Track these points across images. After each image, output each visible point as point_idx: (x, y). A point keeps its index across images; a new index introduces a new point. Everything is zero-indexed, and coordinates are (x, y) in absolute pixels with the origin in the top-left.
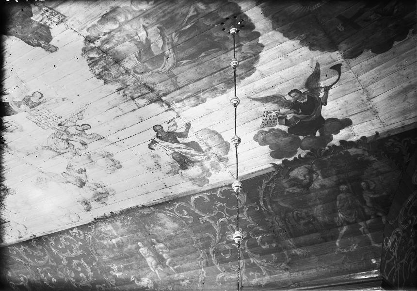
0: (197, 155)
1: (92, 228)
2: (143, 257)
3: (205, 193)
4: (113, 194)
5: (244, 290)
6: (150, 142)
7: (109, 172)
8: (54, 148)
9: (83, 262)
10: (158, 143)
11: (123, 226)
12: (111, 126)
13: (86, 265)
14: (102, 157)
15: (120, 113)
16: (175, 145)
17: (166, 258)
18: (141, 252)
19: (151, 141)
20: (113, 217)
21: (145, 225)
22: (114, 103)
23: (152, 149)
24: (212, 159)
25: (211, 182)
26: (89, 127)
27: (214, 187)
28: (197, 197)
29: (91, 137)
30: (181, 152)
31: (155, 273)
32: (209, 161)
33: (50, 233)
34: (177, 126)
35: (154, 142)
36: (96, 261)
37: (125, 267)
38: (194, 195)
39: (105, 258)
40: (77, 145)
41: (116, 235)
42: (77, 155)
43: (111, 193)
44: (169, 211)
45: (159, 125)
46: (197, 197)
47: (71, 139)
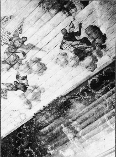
0: (88, 48)
1: (34, 122)
2: (65, 135)
3: (96, 76)
4: (44, 92)
5: (114, 147)
6: (60, 44)
7: (40, 74)
8: (8, 61)
9: (30, 149)
10: (65, 43)
11: (52, 115)
12: (38, 36)
13: (32, 151)
14: (35, 63)
15: (42, 24)
16: (75, 43)
17: (79, 131)
18: (63, 131)
19: (61, 43)
20: (45, 110)
21: (64, 110)
22: (38, 15)
23: (62, 49)
24: (97, 48)
25: (98, 66)
26: (26, 39)
27: (101, 69)
28: (91, 80)
29: (28, 47)
30: (79, 47)
31: (74, 144)
32: (95, 50)
33: (11, 133)
34: (74, 27)
35: (63, 43)
36: (37, 146)
37: (55, 146)
38: (89, 79)
39: (43, 142)
40: (20, 55)
41: (48, 123)
42: (21, 65)
43: (42, 91)
44: (76, 96)
45: (64, 29)
46: (91, 80)
47: (17, 51)
